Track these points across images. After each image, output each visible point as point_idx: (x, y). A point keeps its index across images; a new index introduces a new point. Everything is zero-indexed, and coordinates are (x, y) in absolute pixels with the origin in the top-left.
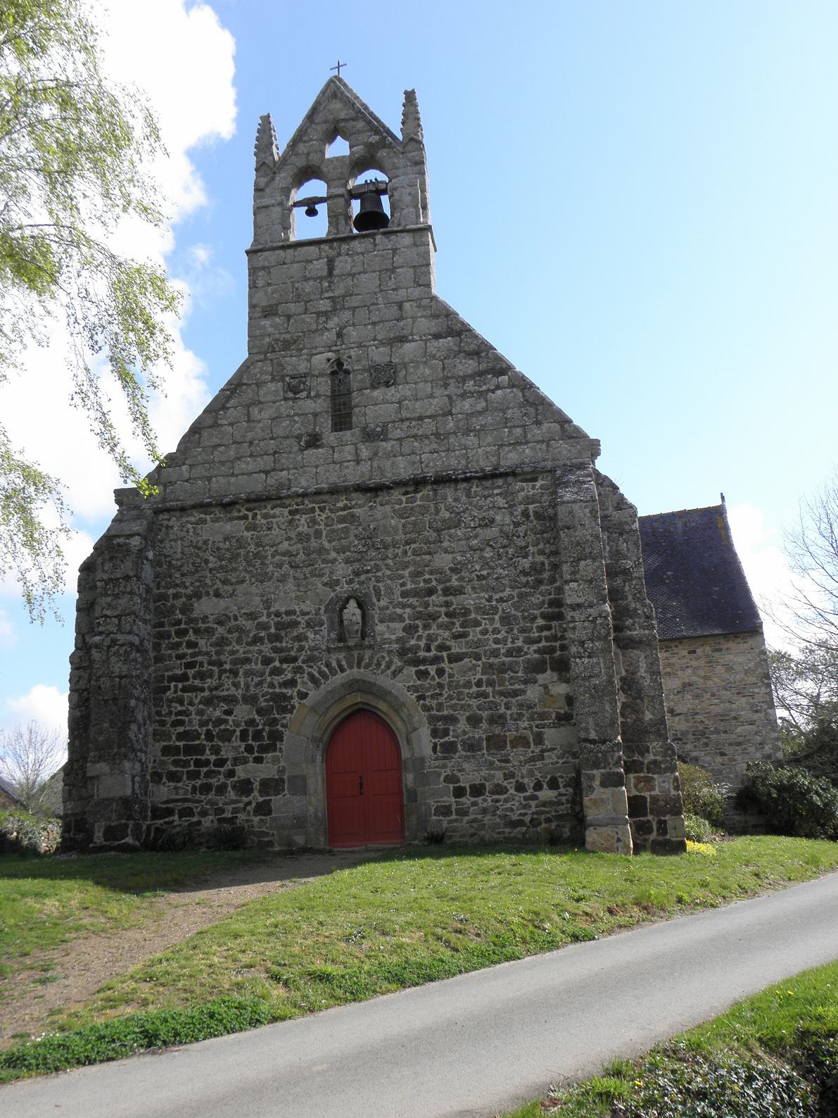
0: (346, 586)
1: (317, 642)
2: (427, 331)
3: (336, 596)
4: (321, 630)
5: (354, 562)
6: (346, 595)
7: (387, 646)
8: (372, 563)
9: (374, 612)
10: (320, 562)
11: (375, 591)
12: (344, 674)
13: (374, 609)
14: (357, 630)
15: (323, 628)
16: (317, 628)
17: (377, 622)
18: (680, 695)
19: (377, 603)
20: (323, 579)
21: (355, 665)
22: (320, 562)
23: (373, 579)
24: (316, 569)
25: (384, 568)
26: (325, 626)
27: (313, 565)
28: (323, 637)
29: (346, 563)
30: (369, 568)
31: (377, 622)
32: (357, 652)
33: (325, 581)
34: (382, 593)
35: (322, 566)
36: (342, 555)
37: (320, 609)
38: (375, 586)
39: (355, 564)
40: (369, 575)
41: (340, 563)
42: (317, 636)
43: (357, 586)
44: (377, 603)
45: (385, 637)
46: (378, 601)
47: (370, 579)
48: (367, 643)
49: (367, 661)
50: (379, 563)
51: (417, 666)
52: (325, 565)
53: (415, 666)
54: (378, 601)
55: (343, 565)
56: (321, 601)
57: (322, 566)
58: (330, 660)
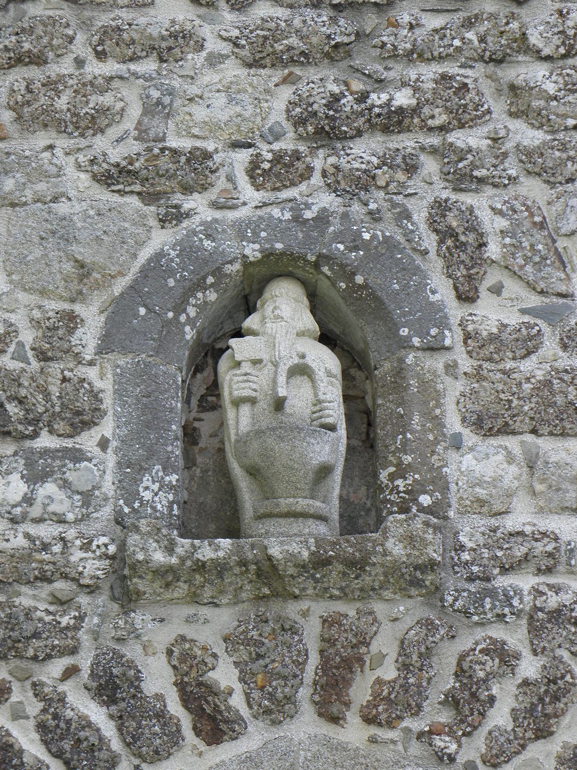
0: (249, 193)
1: (46, 531)
2: (404, 619)
3: (187, 249)
4: (77, 456)
5: (305, 58)
6: (252, 251)
7: (525, 582)
8: (429, 72)
9: (438, 363)
10: (81, 47)
11: (445, 234)
12: (227, 751)
13: (435, 348)
14: (325, 471)
15: (88, 441)
16: (45, 441)
17: (454, 423)
18: (6, 104)
19: (455, 311)
20: (101, 143)
21: (304, 693)
22: (81, 47)
23: (430, 166)
24: (53, 85)
25: (498, 107)
26: (107, 428)
27: (38, 60)
28: (87, 497)
29: (254, 64)
30: (403, 99)
31: (454, 423)
32: (321, 608)
33: (116, 155)
34: (493, 250)
35: (95, 68)
36: (228, 16)
37: (71, 321)
38: (441, 207)
39: (313, 73)
40: (407, 142)
41: (214, 60)
42: (50, 488)
43: (326, 200)
44: (455, 311)
45: (511, 523)
46: (466, 297)
47: (411, 169)
48: (397, 549)
49: (389, 672)
50: (475, 75)
51: (336, 43)
52: (111, 67)
53: (338, 42)
54: (466, 297)
55: (232, 70)
56: (83, 269)
57: (95, 68)
58: (132, 651)
